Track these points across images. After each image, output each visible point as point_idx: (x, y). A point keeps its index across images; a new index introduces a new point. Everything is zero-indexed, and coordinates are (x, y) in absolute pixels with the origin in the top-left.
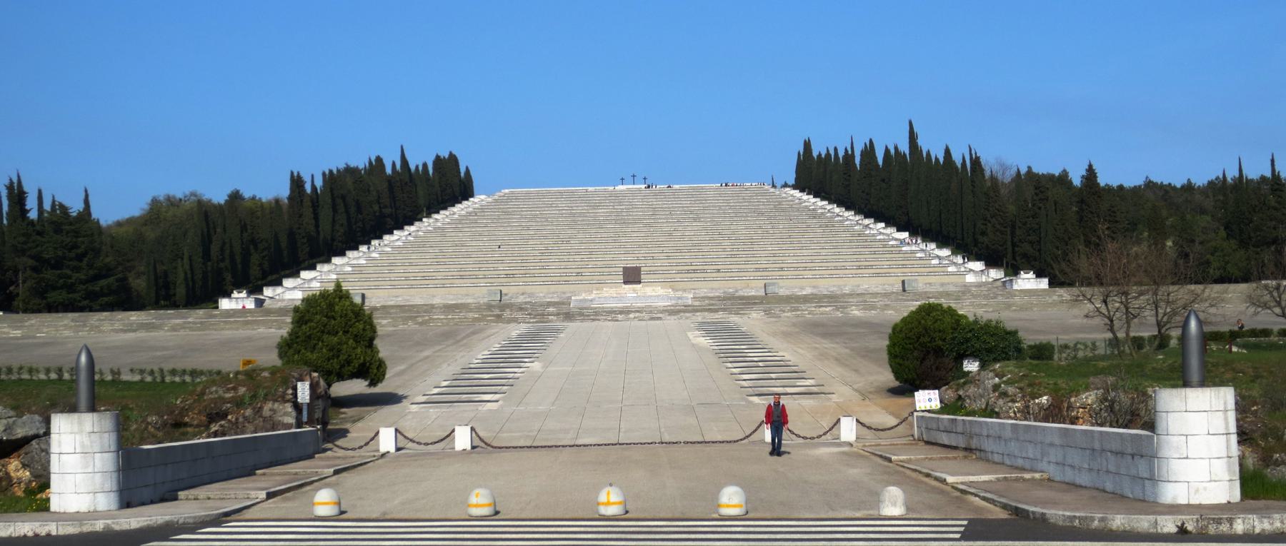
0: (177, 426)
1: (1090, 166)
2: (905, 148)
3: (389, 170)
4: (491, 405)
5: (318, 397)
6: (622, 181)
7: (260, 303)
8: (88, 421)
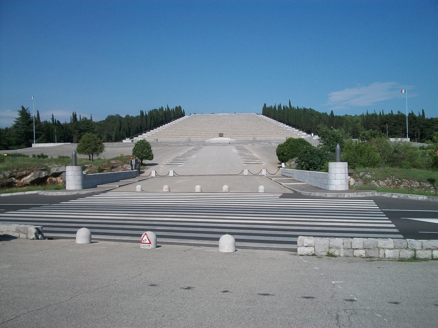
0: (101, 170)
2: (288, 106)
3: (164, 110)
4: (182, 165)
5: (138, 163)
6: (221, 113)
7: (132, 141)
8: (75, 168)
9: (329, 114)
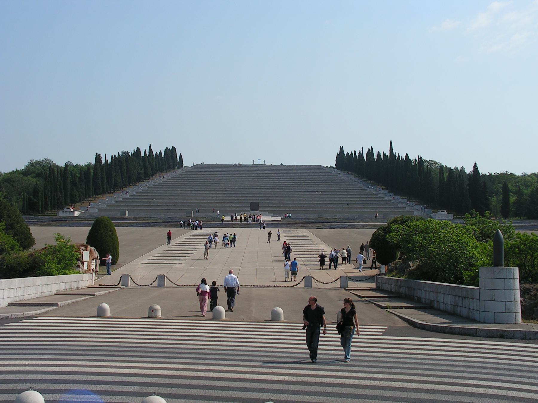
1: (475, 164)
2: (388, 153)
9: (469, 170)
